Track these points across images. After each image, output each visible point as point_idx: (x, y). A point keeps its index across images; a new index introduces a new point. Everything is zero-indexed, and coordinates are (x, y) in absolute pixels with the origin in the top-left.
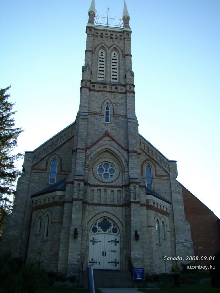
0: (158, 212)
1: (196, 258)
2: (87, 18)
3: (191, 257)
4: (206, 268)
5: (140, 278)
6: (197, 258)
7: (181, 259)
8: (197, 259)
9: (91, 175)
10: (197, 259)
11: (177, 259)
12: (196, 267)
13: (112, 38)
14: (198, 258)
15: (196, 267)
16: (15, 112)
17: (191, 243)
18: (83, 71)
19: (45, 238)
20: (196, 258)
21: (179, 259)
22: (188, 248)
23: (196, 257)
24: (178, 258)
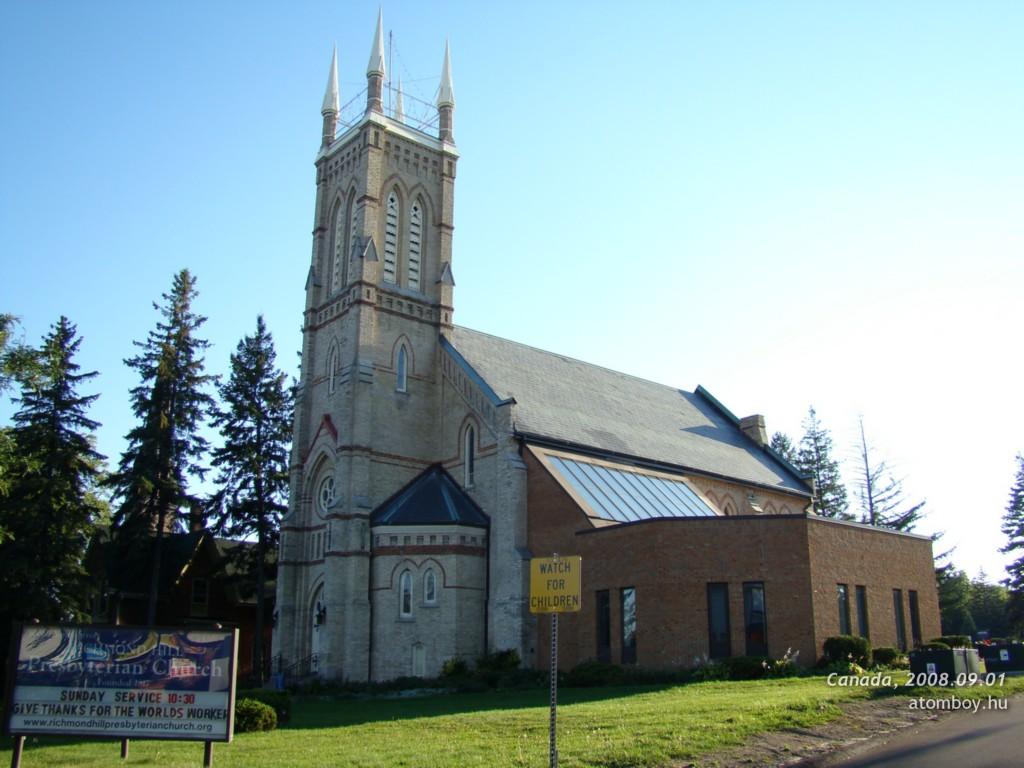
0: (408, 554)
1: (939, 678)
2: (319, 122)
3: (922, 676)
4: (976, 708)
5: (237, 631)
6: (942, 678)
7: (887, 681)
8: (943, 682)
9: (58, 661)
10: (943, 682)
11: (875, 681)
12: (941, 703)
13: (397, 157)
14: (946, 679)
15: (941, 703)
16: (87, 398)
17: (518, 604)
18: (323, 180)
19: (331, 392)
20: (939, 678)
21: (881, 683)
22: (513, 616)
23: (942, 676)
24: (879, 679)
